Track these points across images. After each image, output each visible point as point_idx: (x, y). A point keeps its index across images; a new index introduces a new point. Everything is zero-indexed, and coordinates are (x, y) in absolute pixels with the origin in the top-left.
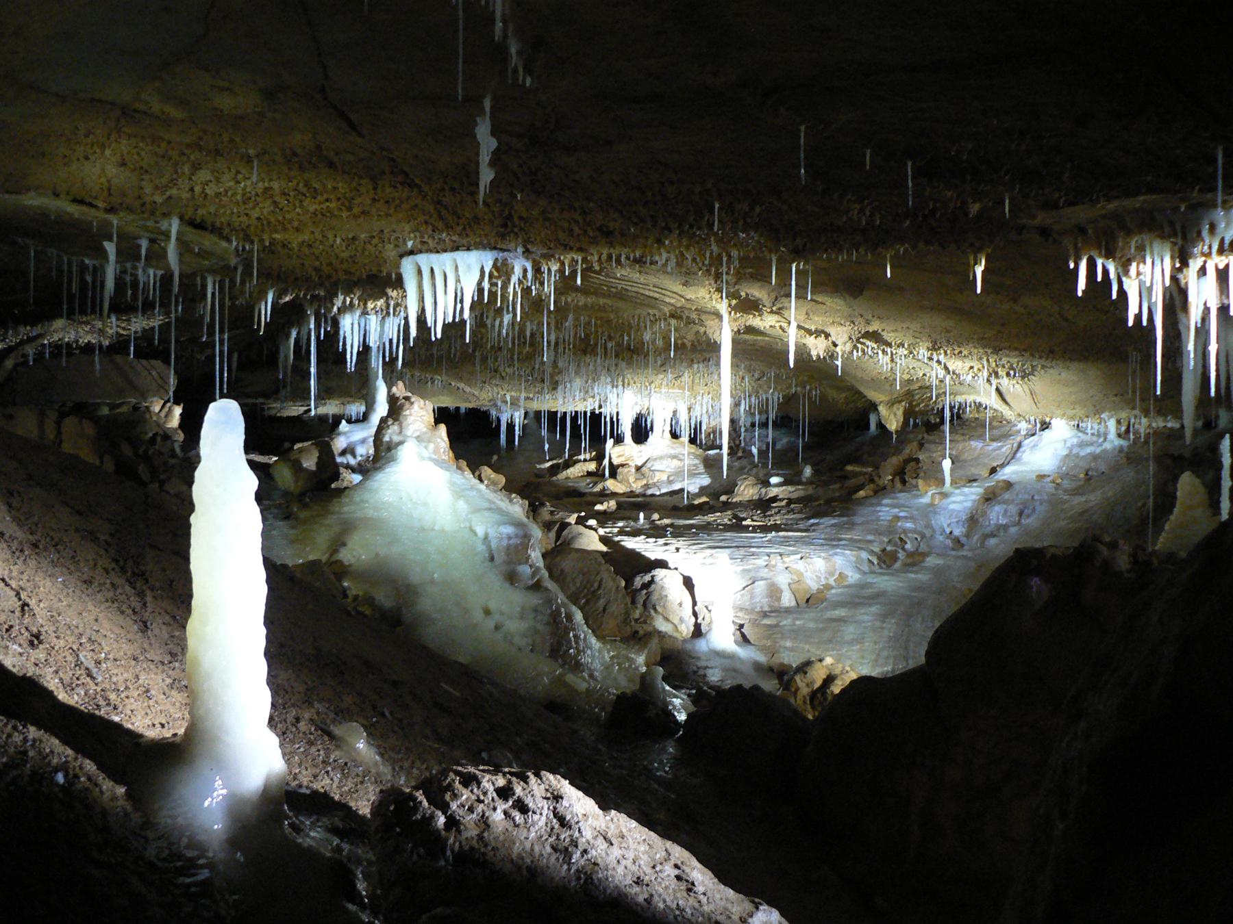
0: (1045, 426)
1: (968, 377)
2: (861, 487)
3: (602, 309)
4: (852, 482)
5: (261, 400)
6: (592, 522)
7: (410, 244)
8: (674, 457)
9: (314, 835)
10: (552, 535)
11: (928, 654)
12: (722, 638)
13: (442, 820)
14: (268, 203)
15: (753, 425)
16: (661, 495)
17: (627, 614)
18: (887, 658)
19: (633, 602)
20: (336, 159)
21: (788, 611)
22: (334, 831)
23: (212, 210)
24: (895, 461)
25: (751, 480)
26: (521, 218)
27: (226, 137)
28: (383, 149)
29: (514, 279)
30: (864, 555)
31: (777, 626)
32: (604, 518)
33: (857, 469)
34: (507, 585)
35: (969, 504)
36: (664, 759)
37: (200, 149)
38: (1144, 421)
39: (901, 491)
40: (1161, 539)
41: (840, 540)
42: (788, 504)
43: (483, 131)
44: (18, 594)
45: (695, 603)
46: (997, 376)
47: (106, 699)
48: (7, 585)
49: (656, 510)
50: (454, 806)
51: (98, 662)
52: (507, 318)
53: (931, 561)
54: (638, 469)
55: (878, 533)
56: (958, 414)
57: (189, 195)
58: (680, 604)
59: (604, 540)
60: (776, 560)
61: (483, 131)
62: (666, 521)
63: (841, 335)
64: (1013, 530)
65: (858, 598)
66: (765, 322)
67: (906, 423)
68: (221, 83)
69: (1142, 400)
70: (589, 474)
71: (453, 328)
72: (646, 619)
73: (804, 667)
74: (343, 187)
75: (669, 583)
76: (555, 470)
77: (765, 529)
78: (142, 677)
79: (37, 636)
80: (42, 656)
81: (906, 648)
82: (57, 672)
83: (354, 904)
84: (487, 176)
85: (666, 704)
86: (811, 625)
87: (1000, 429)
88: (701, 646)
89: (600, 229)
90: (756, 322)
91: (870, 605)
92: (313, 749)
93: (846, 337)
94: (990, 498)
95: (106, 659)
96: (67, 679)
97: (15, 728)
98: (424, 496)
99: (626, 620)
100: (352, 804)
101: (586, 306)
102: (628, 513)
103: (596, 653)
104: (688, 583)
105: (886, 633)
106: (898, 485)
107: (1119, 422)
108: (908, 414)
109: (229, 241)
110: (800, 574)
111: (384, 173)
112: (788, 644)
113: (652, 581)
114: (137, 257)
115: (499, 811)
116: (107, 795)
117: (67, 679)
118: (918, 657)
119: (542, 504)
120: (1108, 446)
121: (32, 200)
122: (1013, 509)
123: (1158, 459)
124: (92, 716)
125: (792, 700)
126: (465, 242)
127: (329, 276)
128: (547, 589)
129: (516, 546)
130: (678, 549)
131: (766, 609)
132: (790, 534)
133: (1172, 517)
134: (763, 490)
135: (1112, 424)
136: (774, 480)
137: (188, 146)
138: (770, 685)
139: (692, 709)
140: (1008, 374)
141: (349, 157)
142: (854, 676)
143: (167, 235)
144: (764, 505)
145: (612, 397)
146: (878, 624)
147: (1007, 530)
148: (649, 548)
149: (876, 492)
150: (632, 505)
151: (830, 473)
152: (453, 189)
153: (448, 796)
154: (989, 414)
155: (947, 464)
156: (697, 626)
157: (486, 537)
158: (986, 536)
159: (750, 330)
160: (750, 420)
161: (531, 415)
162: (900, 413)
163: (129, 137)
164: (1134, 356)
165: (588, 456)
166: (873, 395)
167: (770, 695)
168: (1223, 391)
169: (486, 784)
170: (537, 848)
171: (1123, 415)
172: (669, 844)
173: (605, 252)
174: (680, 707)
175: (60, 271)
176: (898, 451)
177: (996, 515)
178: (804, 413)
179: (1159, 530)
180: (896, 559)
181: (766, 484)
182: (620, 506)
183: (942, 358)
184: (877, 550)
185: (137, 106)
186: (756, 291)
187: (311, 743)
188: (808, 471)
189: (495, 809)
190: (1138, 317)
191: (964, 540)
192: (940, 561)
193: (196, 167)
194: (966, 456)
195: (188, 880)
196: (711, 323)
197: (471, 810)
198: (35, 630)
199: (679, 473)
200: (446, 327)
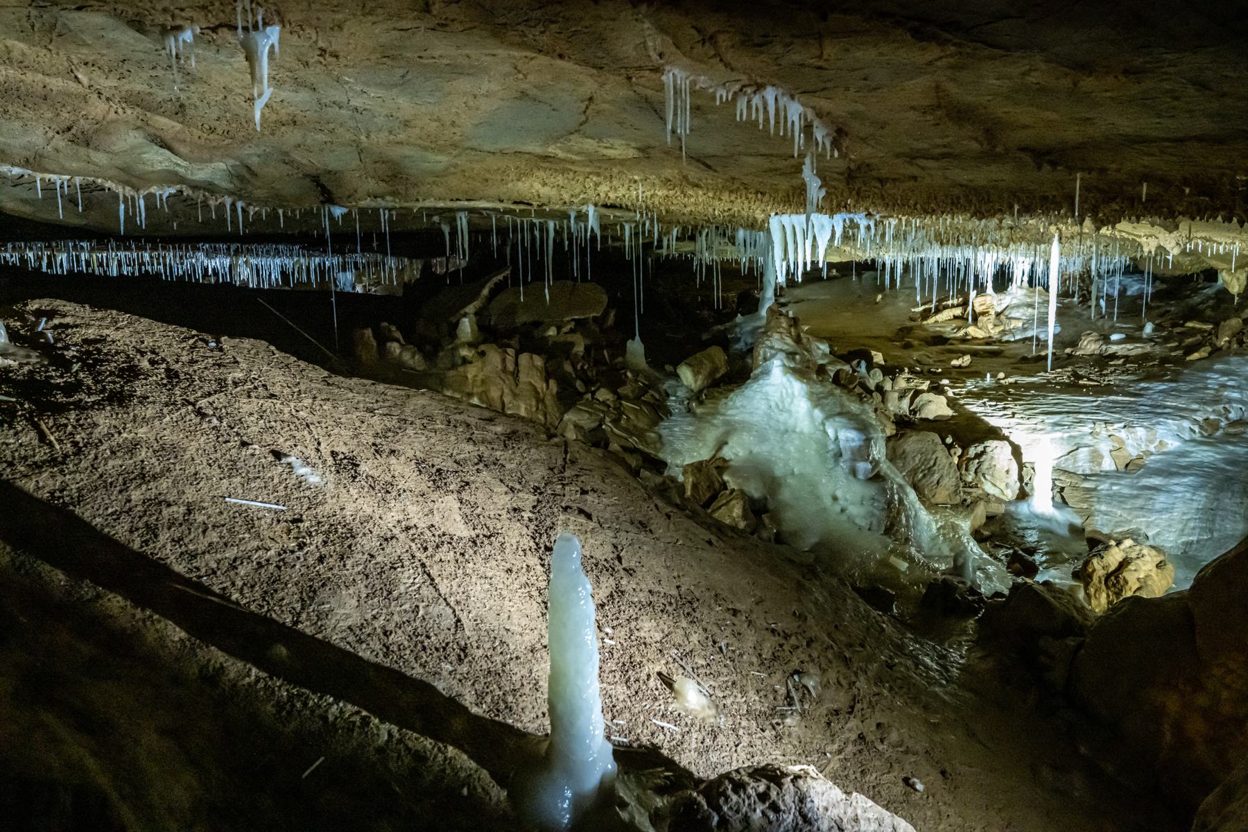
12: (1042, 503)
13: (716, 818)
16: (1016, 342)
18: (1194, 528)
21: (1107, 475)
30: (1186, 424)
31: (1095, 490)
33: (1198, 326)
39: (1236, 354)
41: (1166, 407)
42: (1124, 364)
50: (725, 808)
54: (998, 315)
58: (1007, 472)
59: (952, 403)
60: (1100, 428)
65: (1171, 468)
70: (955, 317)
86: (1126, 491)
91: (1184, 475)
93: (1173, 243)
100: (676, 758)
103: (926, 523)
104: (1016, 452)
105: (1195, 505)
110: (1122, 442)
112: (1103, 508)
115: (758, 811)
116: (494, 799)
130: (1014, 414)
131: (1088, 472)
132: (1120, 398)
134: (1104, 347)
136: (1114, 337)
144: (1102, 361)
146: (1188, 495)
151: (1169, 328)
156: (1022, 489)
165: (955, 302)
169: (750, 791)
181: (1106, 339)
184: (1200, 419)
188: (1149, 328)
189: (755, 810)
193: (597, 185)
197: (737, 811)
200: (805, 273)
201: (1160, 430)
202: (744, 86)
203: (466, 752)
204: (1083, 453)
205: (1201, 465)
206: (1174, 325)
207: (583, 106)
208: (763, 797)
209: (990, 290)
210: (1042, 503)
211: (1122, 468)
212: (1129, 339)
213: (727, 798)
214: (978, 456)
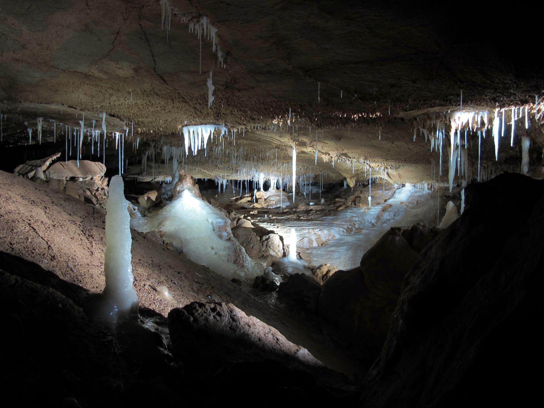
0: (403, 186)
1: (378, 169)
2: (341, 206)
3: (252, 145)
4: (337, 204)
5: (136, 176)
6: (249, 218)
7: (186, 122)
8: (277, 196)
9: (149, 324)
10: (235, 222)
11: (361, 263)
12: (293, 256)
13: (192, 319)
14: (137, 107)
15: (304, 185)
17: (260, 249)
18: (349, 264)
19: (262, 245)
20: (159, 93)
21: (315, 248)
22: (156, 323)
23: (117, 110)
24: (352, 197)
25: (303, 204)
26: (223, 114)
27: (121, 85)
28: (175, 89)
29: (222, 135)
30: (341, 229)
31: (311, 253)
32: (253, 216)
34: (219, 239)
35: (377, 212)
36: (273, 299)
37: (112, 89)
38: (437, 184)
40: (441, 224)
43: (210, 83)
44: (47, 243)
45: (283, 245)
46: (387, 168)
47: (77, 278)
48: (43, 239)
49: (271, 214)
50: (196, 314)
51: (75, 266)
52: (220, 148)
53: (364, 231)
54: (265, 200)
55: (346, 221)
56: (374, 182)
57: (109, 105)
59: (252, 224)
60: (311, 231)
61: (210, 83)
62: (274, 218)
63: (334, 155)
64: (392, 221)
65: (338, 244)
66: (309, 150)
67: (356, 184)
68: (119, 66)
69: (436, 177)
70: (249, 201)
71: (201, 151)
72: (267, 251)
73: (320, 267)
74: (162, 103)
75: (275, 239)
76: (237, 200)
77: (308, 220)
78: (90, 271)
79: (54, 257)
80: (55, 264)
81: (355, 261)
82: (60, 269)
83: (162, 347)
84: (211, 99)
85: (273, 280)
86: (323, 253)
87: (387, 186)
88: (285, 260)
89: (251, 118)
90: (305, 150)
91: (343, 246)
92: (150, 295)
93: (335, 155)
94: (384, 210)
95: (78, 265)
96: (64, 272)
97: (45, 289)
98: (190, 211)
99: (260, 251)
101: (246, 144)
102: (261, 215)
103: (249, 262)
104: (281, 238)
105: (348, 256)
106: (353, 205)
107: (428, 184)
108: (357, 182)
109: (123, 121)
111: (176, 98)
113: (269, 238)
114: (92, 127)
117: (64, 272)
118: (358, 265)
119: (232, 212)
120: (424, 192)
121: (53, 107)
122: (392, 214)
123: (441, 197)
124: (72, 284)
125: (316, 278)
126: (204, 122)
127: (158, 134)
128: (233, 240)
129: (222, 226)
133: (444, 217)
135: (426, 185)
136: (311, 204)
137: (108, 88)
138: (308, 273)
139: (282, 281)
140: (391, 168)
141: (164, 92)
142: (337, 270)
143: (102, 119)
144: (308, 212)
145: (257, 175)
146: (345, 252)
147: (390, 221)
148: (269, 227)
149: (346, 208)
150: (263, 212)
151: (331, 201)
152: (200, 104)
153: (194, 311)
154: (384, 181)
155: (370, 198)
156: (284, 253)
157: (212, 223)
158: (383, 223)
159: (303, 152)
160: (303, 183)
161: (229, 181)
162: (354, 181)
163: (88, 84)
164: (433, 162)
166: (345, 175)
167: (309, 277)
168: (462, 174)
169: (207, 307)
170: (224, 329)
171: (430, 182)
172: (271, 327)
173: (253, 125)
174: (278, 280)
175: (65, 132)
176: (353, 194)
177: (386, 216)
178: (321, 181)
179: (440, 221)
180: (352, 231)
181: (309, 205)
182: (259, 212)
183: (368, 162)
184: (346, 227)
185: (90, 74)
186: (305, 139)
187: (149, 293)
188: (323, 201)
189: (210, 315)
190: (434, 149)
191: (375, 224)
192: (367, 231)
193: (111, 95)
194: (376, 196)
195: (105, 340)
196: (289, 150)
198: (53, 255)
199: (279, 201)
200: (198, 151)
201: (333, 231)
202: (193, 18)
203: (59, 291)
204: (306, 240)
205: (347, 242)
206: (331, 200)
207: (113, 37)
208: (213, 310)
209: (262, 189)
210: (293, 256)
211: (320, 245)
212: (315, 204)
213: (197, 311)
214: (267, 239)
